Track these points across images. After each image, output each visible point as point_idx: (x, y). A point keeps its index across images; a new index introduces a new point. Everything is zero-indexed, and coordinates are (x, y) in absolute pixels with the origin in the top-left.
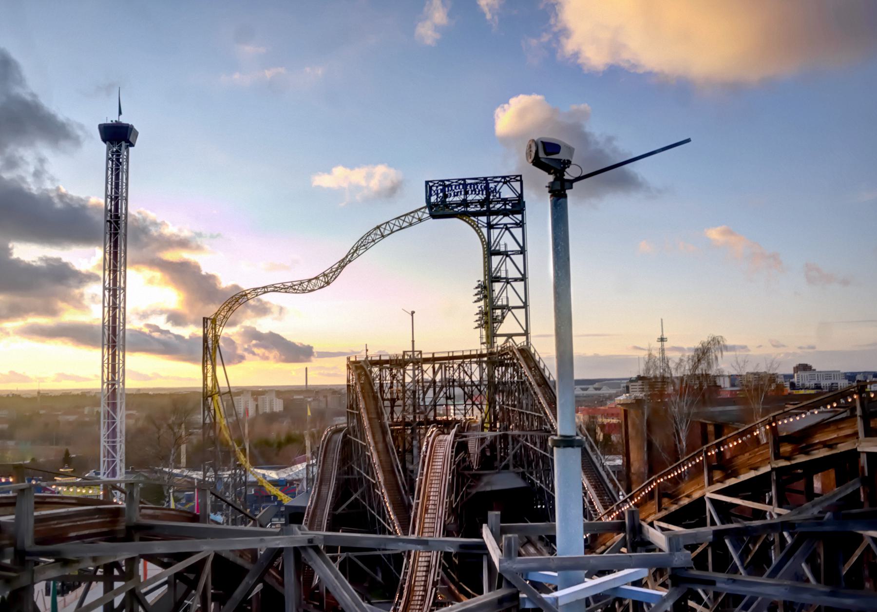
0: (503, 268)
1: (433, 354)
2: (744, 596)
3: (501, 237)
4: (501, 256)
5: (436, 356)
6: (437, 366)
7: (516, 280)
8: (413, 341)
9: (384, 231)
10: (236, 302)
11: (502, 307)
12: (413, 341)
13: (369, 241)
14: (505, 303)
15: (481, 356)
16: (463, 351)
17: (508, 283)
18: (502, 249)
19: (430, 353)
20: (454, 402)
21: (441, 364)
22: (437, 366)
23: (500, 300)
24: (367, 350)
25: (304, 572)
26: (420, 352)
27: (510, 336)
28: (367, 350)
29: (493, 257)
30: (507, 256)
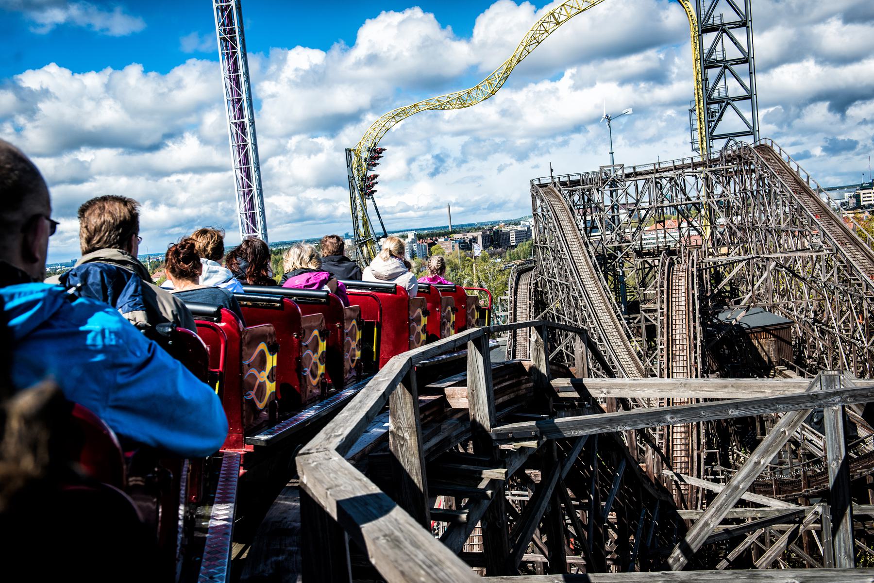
0: (719, 47)
1: (634, 168)
2: (816, 457)
3: (714, 7)
4: (716, 33)
5: (638, 170)
6: (641, 184)
7: (738, 62)
8: (382, 224)
9: (559, 17)
10: (430, 109)
11: (719, 101)
12: (382, 224)
13: (541, 32)
14: (723, 94)
15: (695, 165)
16: (683, 160)
17: (726, 67)
18: (717, 22)
19: (630, 167)
20: (664, 227)
21: (647, 181)
22: (641, 184)
23: (716, 91)
24: (552, 170)
25: (647, 430)
26: (622, 167)
27: (729, 136)
28: (552, 170)
29: (704, 35)
30: (724, 31)
